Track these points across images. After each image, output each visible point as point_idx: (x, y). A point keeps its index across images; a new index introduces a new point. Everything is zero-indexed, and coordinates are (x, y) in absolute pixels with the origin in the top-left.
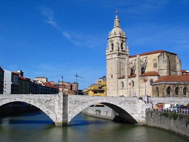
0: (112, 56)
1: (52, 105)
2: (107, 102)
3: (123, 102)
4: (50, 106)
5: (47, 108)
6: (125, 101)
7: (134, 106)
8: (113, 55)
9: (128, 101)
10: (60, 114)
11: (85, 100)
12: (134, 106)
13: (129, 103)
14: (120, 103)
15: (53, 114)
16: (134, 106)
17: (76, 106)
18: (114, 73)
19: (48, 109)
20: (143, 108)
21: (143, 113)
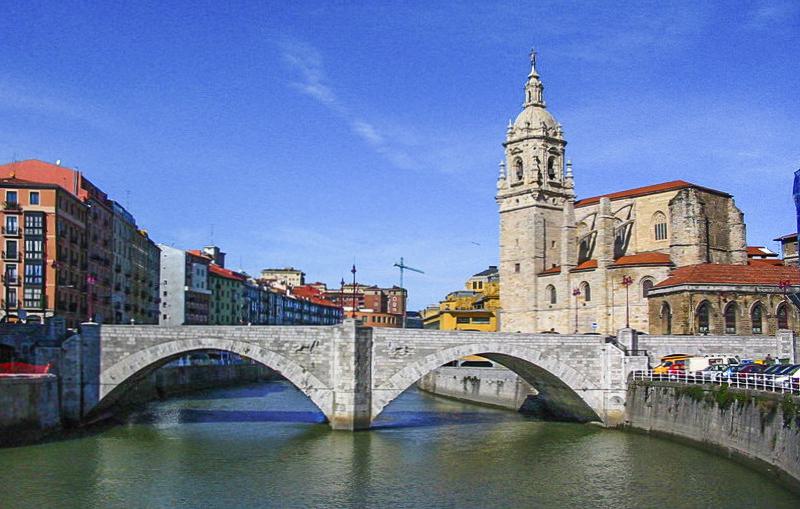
0: (518, 201)
1: (320, 362)
4: (313, 364)
5: (304, 371)
6: (558, 347)
7: (587, 366)
8: (520, 197)
9: (569, 348)
11: (428, 345)
12: (587, 366)
13: (574, 355)
15: (323, 391)
19: (307, 373)
20: (619, 372)
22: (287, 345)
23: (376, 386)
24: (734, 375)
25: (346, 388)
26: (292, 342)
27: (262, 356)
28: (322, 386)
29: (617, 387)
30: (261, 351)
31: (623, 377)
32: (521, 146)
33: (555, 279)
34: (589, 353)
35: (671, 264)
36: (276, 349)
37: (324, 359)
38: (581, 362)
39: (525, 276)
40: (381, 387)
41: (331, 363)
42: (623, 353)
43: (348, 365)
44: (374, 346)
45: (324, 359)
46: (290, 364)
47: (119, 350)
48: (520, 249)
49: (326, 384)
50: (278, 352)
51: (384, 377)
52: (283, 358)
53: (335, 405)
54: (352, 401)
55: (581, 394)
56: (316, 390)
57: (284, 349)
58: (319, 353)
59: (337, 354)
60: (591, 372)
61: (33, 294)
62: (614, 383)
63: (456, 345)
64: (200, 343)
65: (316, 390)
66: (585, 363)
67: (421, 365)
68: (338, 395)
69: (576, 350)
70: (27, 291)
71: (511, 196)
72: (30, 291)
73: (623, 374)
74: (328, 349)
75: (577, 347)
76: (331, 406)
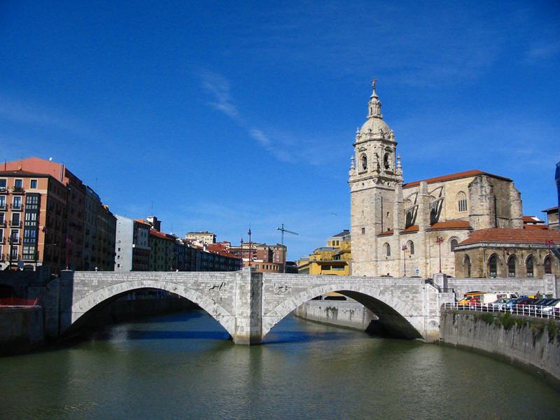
0: (363, 184)
2: (353, 290)
3: (388, 288)
4: (221, 298)
5: (215, 303)
6: (392, 286)
7: (413, 299)
8: (365, 182)
9: (400, 287)
10: (244, 317)
12: (413, 299)
14: (382, 293)
16: (415, 299)
17: (280, 298)
18: (369, 222)
19: (217, 305)
21: (433, 314)
22: (203, 285)
23: (265, 314)
24: (515, 306)
25: (244, 315)
26: (207, 283)
27: (186, 293)
28: (227, 313)
29: (433, 314)
30: (185, 289)
31: (437, 307)
32: (365, 146)
33: (389, 239)
34: (414, 291)
35: (470, 229)
36: (195, 288)
37: (229, 295)
38: (408, 297)
39: (369, 236)
40: (269, 314)
41: (233, 297)
42: (437, 291)
43: (246, 299)
44: (264, 285)
45: (229, 295)
46: (205, 298)
47: (86, 289)
48: (365, 218)
49: (230, 312)
50: (197, 290)
51: (270, 307)
52: (200, 294)
53: (237, 327)
54: (249, 324)
55: (409, 319)
56: (223, 316)
57: (201, 288)
58: (225, 291)
59: (238, 291)
60: (415, 303)
61: (29, 250)
62: (431, 312)
63: (321, 285)
64: (142, 284)
65: (223, 316)
66: (411, 297)
67: (296, 299)
68: (239, 320)
69: (405, 289)
70: (25, 248)
71: (359, 181)
72: (27, 248)
73: (437, 305)
74: (232, 288)
75: (405, 286)
76: (233, 327)
